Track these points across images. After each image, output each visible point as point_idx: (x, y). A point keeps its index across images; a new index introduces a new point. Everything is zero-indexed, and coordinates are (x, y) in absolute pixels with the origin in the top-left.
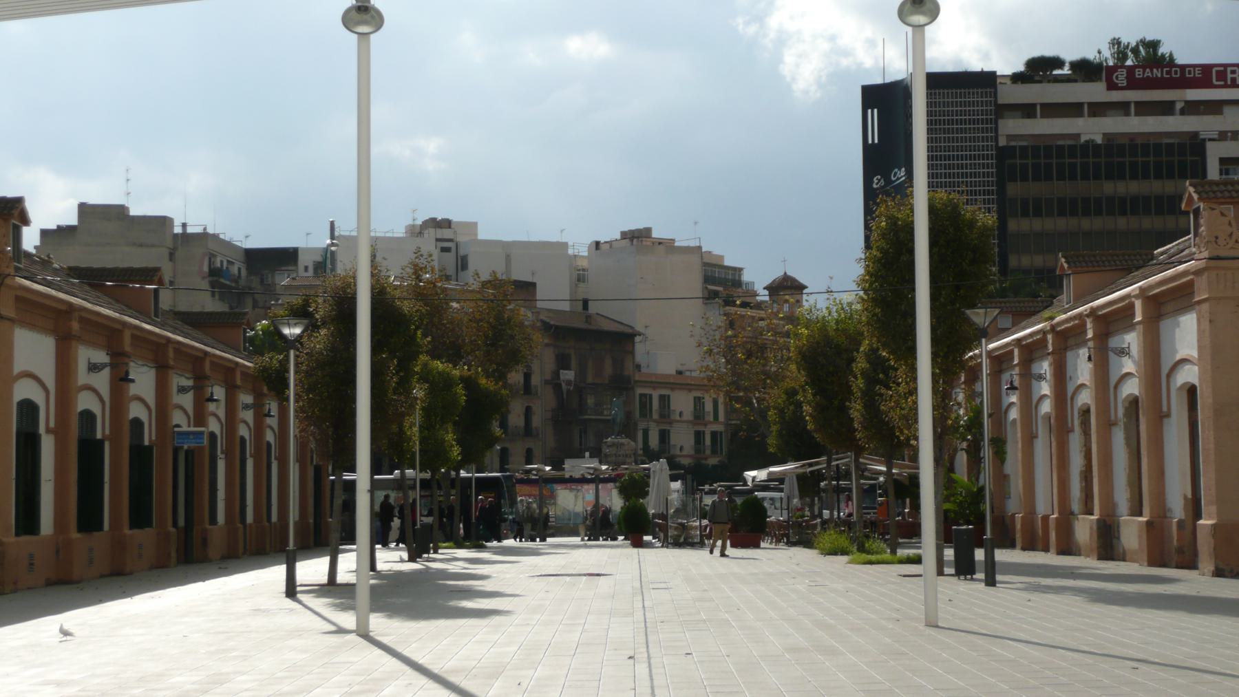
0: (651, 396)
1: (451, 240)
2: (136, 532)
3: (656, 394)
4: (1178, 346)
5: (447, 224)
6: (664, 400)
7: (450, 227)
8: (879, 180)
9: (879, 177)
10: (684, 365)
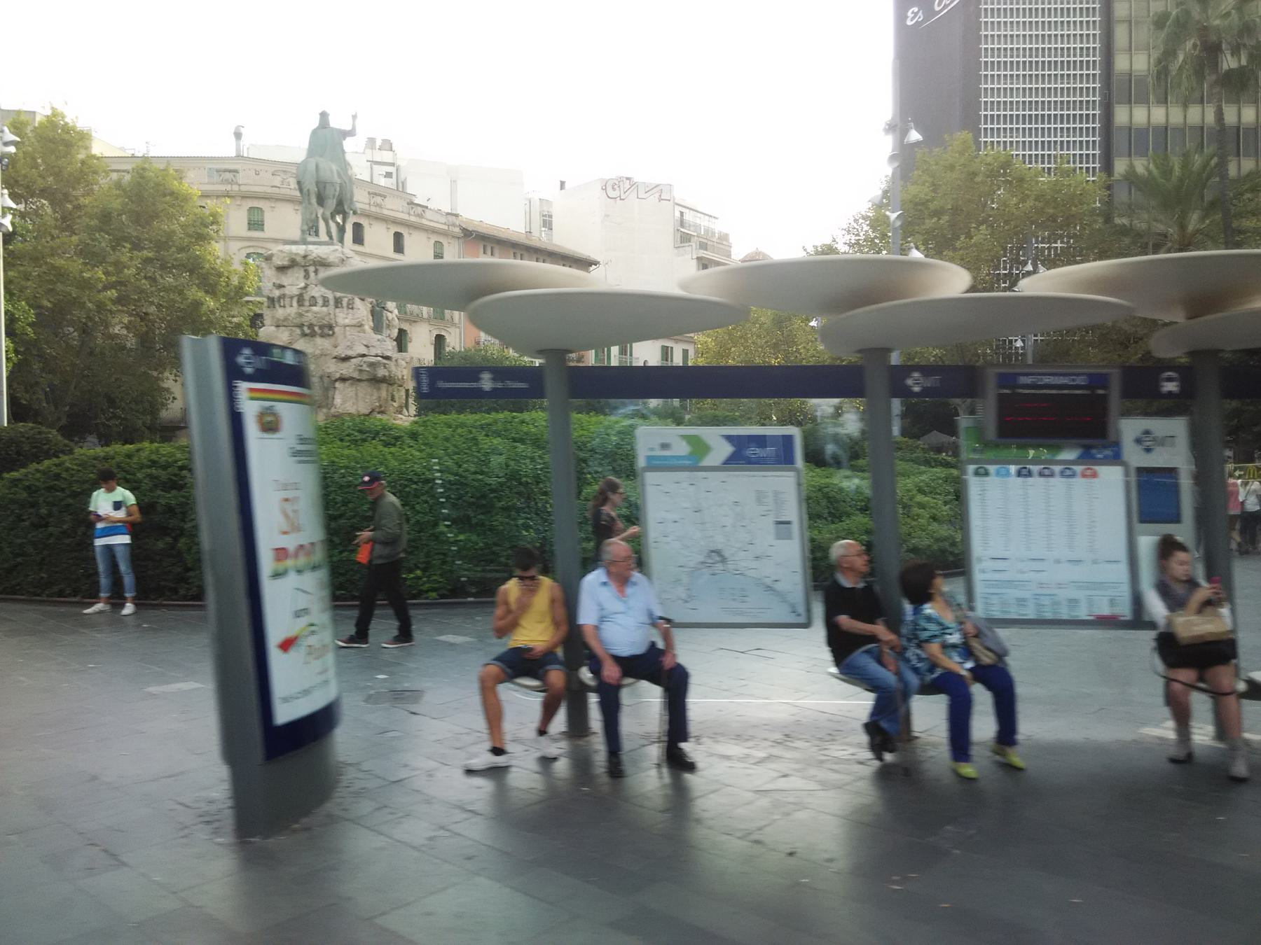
1: (393, 165)
5: (388, 146)
7: (391, 150)
8: (916, 14)
9: (916, 9)
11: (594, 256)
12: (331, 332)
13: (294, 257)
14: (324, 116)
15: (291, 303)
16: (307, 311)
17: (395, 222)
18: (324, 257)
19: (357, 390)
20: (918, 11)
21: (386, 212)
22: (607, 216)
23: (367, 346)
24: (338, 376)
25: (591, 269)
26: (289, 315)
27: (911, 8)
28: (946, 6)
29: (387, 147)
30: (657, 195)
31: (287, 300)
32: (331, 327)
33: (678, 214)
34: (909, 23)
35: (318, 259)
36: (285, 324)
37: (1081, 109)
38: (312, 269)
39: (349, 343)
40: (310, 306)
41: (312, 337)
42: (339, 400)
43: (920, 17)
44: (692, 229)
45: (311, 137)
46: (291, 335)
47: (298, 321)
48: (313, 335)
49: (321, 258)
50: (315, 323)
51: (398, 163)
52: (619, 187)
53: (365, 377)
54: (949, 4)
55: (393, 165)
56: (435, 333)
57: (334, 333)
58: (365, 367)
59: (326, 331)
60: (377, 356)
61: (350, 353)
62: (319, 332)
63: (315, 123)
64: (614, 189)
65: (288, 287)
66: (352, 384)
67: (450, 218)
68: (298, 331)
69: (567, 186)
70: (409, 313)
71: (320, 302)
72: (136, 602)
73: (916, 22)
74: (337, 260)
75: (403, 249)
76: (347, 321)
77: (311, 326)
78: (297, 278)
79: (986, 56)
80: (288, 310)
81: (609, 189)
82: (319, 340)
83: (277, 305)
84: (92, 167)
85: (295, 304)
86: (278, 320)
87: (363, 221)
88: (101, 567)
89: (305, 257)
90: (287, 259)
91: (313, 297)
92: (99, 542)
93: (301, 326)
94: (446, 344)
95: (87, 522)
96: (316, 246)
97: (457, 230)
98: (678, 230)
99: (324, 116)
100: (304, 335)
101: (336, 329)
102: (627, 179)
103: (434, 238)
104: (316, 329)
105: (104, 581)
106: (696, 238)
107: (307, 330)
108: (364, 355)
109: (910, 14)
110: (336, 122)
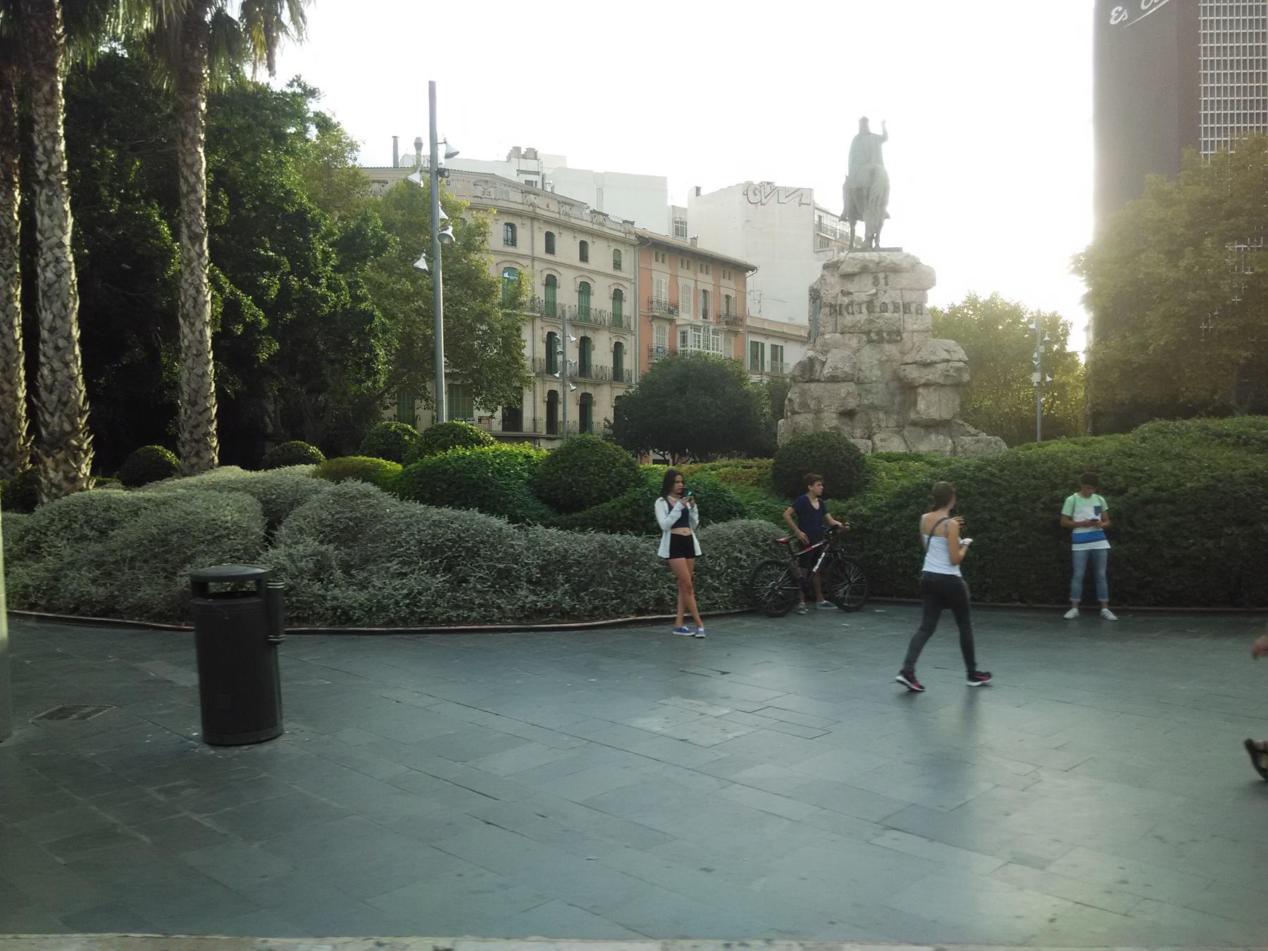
0: (763, 345)
1: (537, 173)
2: (39, 510)
3: (768, 344)
4: (1090, 518)
5: (532, 154)
6: (777, 352)
7: (536, 158)
8: (1120, 13)
9: (1120, 8)
10: (793, 319)
11: (750, 261)
12: (899, 338)
13: (867, 263)
14: (864, 122)
15: (860, 310)
16: (878, 318)
17: (583, 231)
18: (898, 262)
19: (939, 395)
20: (1122, 12)
21: (573, 221)
22: (748, 221)
23: (948, 351)
24: (923, 381)
25: (748, 274)
26: (859, 321)
27: (1114, 7)
28: (1154, 5)
29: (533, 156)
30: (797, 200)
31: (856, 308)
32: (899, 333)
33: (816, 219)
34: (1113, 22)
35: (893, 265)
36: (852, 330)
37: (1225, 109)
38: (881, 276)
39: (931, 349)
40: (881, 312)
41: (879, 343)
42: (923, 407)
43: (1125, 16)
44: (829, 233)
45: (853, 142)
46: (859, 342)
47: (865, 328)
48: (881, 341)
49: (895, 264)
50: (885, 329)
51: (544, 171)
52: (760, 192)
53: (949, 382)
54: (1158, 3)
55: (537, 173)
56: (615, 340)
57: (902, 339)
58: (952, 372)
59: (894, 337)
60: (960, 361)
61: (934, 358)
62: (887, 338)
63: (855, 131)
64: (755, 195)
65: (855, 294)
66: (935, 390)
67: (627, 226)
68: (865, 338)
69: (703, 192)
70: (593, 321)
71: (891, 307)
72: (1113, 607)
73: (1121, 20)
74: (909, 266)
75: (587, 257)
76: (916, 327)
77: (879, 333)
78: (866, 285)
79: (1205, 55)
80: (858, 317)
81: (750, 193)
82: (887, 347)
83: (845, 313)
84: (357, 177)
85: (864, 310)
86: (846, 326)
87: (554, 230)
88: (1079, 572)
89: (878, 263)
90: (858, 266)
91: (884, 303)
92: (1077, 548)
93: (868, 333)
94: (624, 351)
95: (1063, 532)
96: (887, 253)
97: (633, 237)
98: (818, 235)
99: (864, 122)
100: (870, 341)
101: (904, 335)
102: (768, 183)
103: (614, 246)
104: (885, 335)
105: (1076, 585)
106: (833, 243)
107: (873, 336)
108: (948, 361)
109: (1113, 13)
110: (875, 128)
